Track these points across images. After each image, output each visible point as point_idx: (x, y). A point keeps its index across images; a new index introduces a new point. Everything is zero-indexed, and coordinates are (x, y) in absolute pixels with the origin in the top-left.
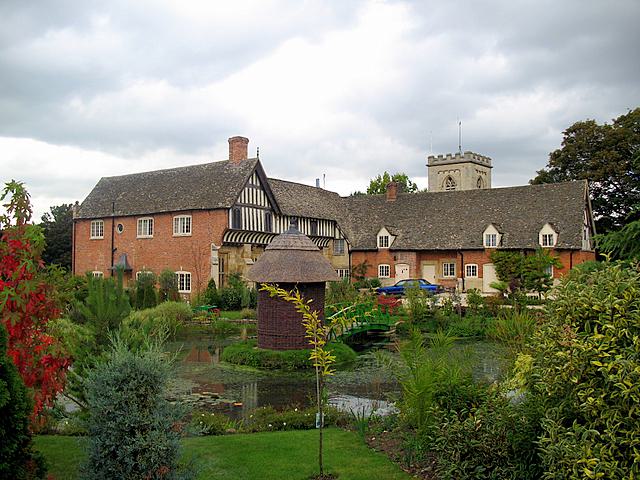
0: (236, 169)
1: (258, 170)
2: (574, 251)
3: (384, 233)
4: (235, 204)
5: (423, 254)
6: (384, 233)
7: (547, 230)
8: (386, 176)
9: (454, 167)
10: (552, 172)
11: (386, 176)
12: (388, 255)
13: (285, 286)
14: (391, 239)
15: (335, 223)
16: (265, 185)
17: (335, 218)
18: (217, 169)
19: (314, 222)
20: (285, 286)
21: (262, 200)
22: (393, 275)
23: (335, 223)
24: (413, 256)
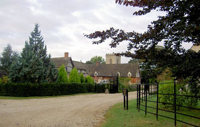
0: (66, 59)
1: (71, 59)
2: (134, 77)
3: (96, 72)
4: (66, 67)
5: (104, 77)
6: (96, 72)
7: (129, 73)
8: (96, 56)
9: (112, 57)
10: (133, 60)
11: (96, 56)
12: (97, 77)
13: (46, 46)
14: (97, 74)
15: (85, 70)
16: (72, 62)
17: (85, 69)
18: (61, 59)
19: (81, 70)
20: (46, 46)
21: (71, 66)
22: (98, 81)
23: (85, 70)
24: (102, 78)
